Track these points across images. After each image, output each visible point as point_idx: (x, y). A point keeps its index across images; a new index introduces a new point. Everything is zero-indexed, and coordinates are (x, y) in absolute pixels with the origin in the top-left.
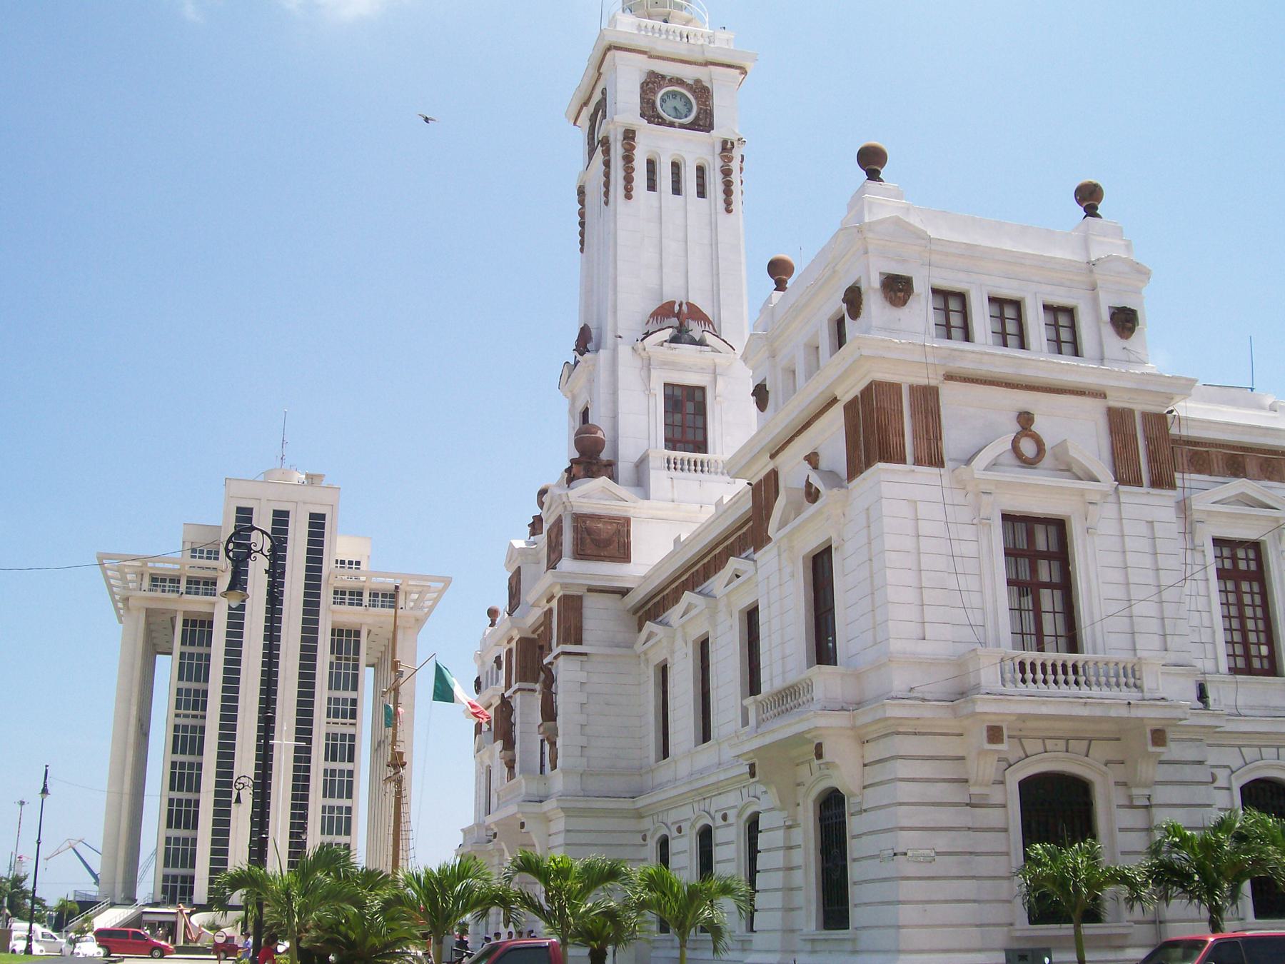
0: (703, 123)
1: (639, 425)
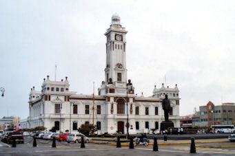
0: (122, 40)
1: (115, 79)
